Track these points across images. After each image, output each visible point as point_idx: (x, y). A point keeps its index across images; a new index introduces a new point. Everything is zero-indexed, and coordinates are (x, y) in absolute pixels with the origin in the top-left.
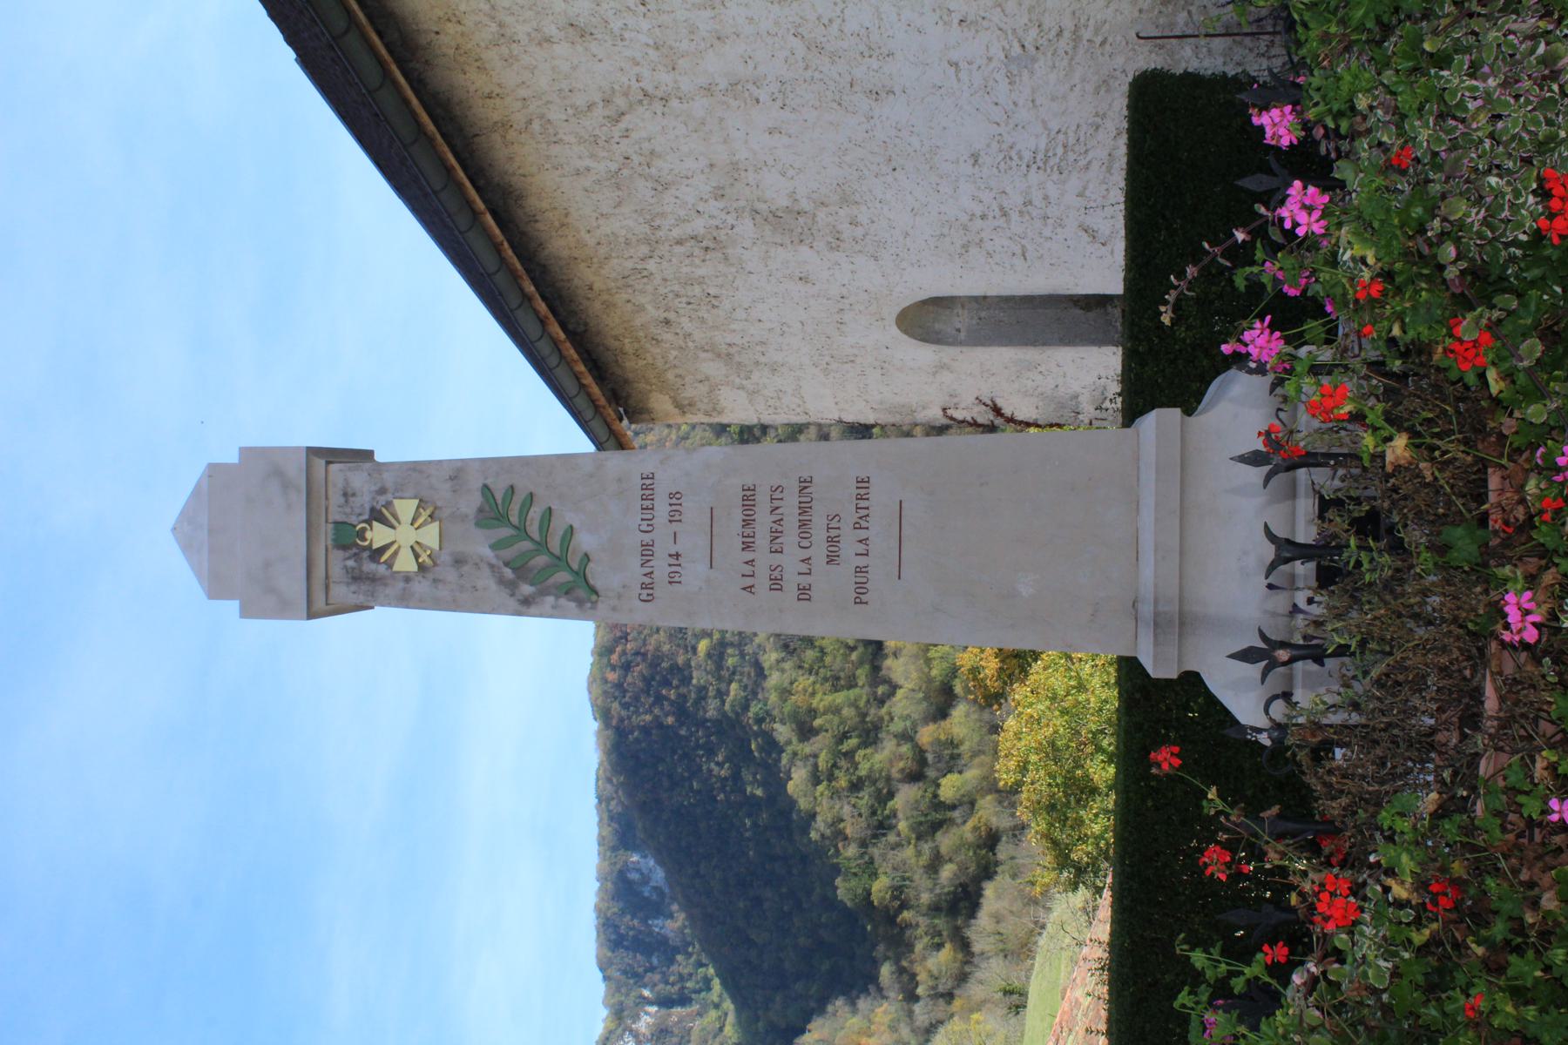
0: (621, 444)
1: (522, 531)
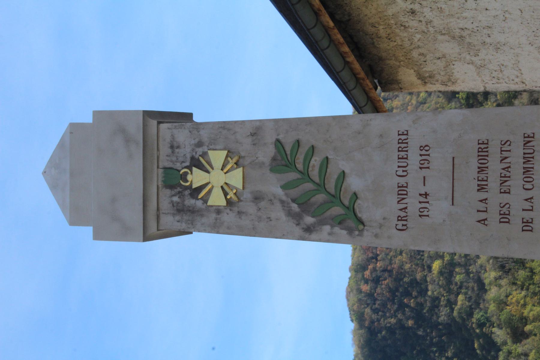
0: (377, 109)
1: (305, 175)
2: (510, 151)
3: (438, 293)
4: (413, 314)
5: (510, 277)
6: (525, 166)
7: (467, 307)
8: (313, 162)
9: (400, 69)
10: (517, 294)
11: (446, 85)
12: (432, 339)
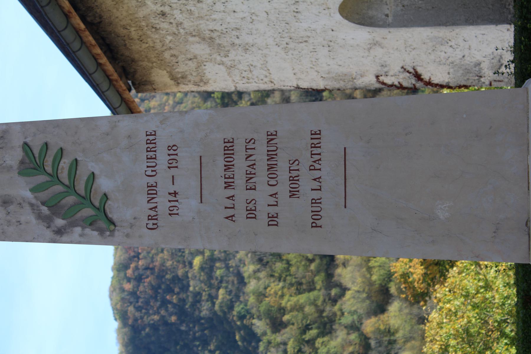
1: (55, 177)
2: (254, 149)
3: (199, 289)
4: (175, 311)
5: (268, 269)
6: (269, 163)
7: (228, 300)
8: (62, 164)
9: (153, 70)
10: (275, 285)
11: (199, 85)
12: (194, 334)
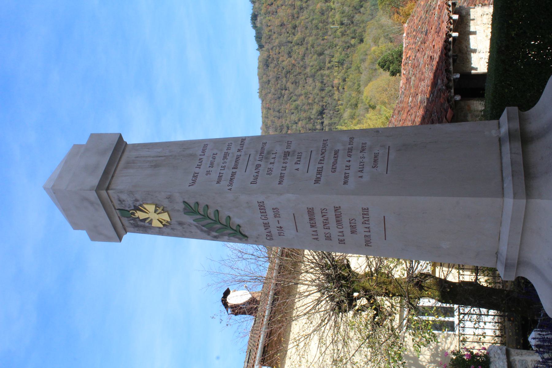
1: (207, 217)
